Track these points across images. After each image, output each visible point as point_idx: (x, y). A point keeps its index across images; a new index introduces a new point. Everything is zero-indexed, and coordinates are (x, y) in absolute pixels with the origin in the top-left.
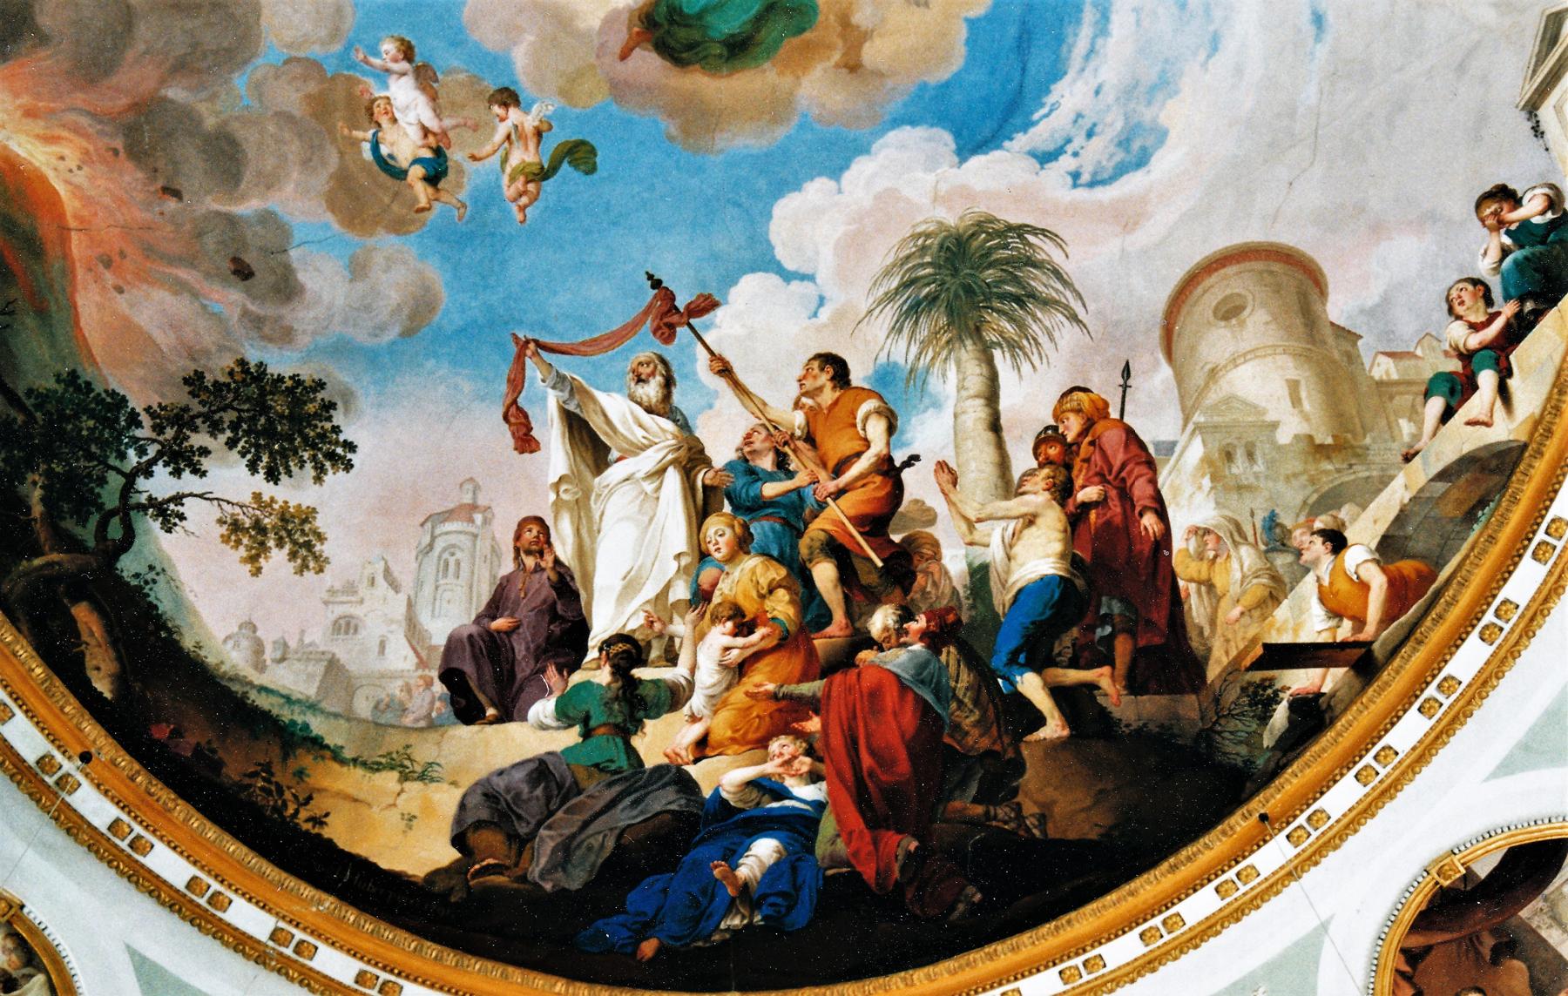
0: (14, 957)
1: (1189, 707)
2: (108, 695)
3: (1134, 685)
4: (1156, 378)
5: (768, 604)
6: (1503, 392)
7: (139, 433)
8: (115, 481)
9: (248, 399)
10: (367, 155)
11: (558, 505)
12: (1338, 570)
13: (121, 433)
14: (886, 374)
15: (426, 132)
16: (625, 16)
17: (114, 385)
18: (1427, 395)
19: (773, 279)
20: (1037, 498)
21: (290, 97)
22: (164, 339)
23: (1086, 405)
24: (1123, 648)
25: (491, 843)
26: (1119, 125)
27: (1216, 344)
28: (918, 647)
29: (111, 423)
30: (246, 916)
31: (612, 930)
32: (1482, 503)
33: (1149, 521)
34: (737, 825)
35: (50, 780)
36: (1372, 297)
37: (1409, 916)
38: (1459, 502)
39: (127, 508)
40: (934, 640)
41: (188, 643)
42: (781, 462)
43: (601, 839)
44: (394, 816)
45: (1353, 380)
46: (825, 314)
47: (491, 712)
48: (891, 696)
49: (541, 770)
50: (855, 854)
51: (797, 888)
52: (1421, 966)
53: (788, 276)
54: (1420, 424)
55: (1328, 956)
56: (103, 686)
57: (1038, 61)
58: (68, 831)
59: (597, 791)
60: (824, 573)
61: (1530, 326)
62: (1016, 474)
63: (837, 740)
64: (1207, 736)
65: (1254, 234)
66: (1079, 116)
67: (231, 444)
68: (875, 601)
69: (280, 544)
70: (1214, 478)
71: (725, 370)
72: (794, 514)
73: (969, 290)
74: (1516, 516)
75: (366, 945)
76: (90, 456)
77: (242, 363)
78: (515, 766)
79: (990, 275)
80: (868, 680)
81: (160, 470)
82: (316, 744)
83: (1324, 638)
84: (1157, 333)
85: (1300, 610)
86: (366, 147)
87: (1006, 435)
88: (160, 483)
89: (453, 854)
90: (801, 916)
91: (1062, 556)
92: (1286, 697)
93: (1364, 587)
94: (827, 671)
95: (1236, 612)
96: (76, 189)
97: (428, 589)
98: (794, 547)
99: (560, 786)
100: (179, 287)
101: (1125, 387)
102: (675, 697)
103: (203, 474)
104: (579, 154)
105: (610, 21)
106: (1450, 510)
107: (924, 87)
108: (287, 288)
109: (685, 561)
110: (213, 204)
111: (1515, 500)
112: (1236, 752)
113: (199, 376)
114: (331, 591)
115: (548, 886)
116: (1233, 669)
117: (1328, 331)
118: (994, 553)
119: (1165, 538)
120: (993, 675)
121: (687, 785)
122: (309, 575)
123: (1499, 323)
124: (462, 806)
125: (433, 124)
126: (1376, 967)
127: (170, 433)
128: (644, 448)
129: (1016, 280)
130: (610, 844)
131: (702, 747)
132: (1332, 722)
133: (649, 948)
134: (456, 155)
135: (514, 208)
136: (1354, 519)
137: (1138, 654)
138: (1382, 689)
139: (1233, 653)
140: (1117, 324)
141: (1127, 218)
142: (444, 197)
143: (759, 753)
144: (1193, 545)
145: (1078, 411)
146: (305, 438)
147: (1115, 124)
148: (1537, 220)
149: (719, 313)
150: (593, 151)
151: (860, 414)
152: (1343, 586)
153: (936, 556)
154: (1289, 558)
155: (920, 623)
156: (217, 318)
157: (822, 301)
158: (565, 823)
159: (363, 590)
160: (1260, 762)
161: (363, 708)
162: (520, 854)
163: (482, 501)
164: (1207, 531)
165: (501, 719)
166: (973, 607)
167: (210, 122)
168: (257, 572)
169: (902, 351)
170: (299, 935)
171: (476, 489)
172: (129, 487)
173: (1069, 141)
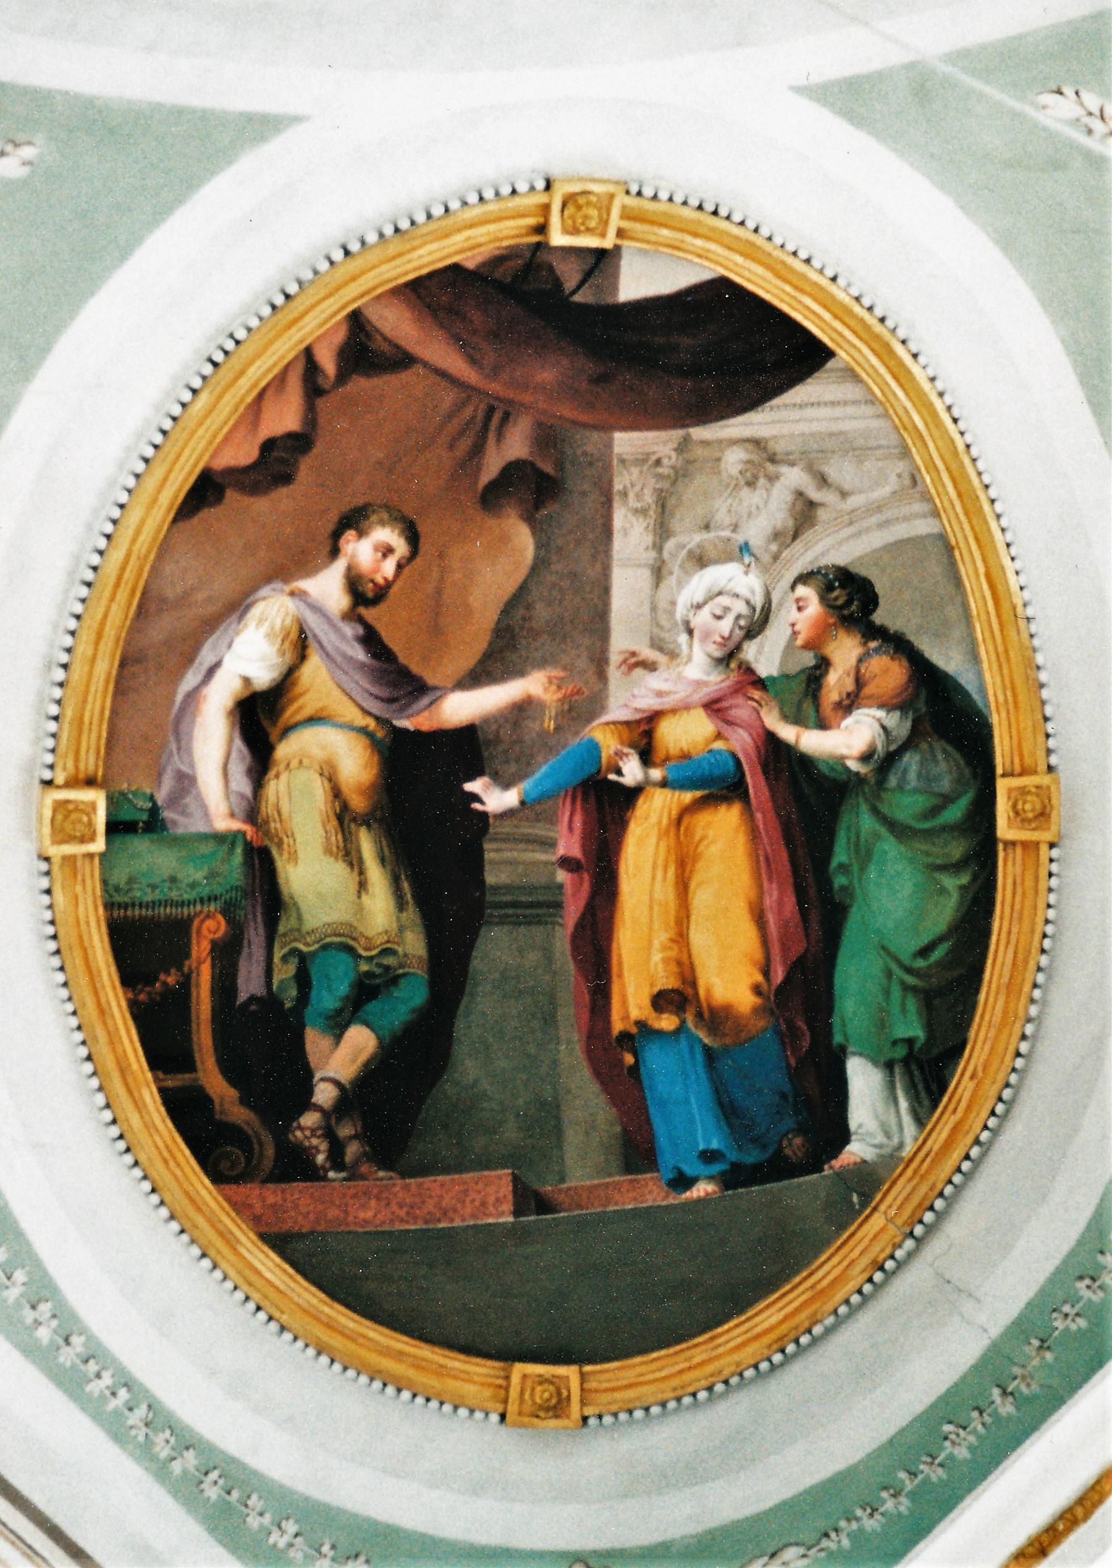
52: (360, 384)
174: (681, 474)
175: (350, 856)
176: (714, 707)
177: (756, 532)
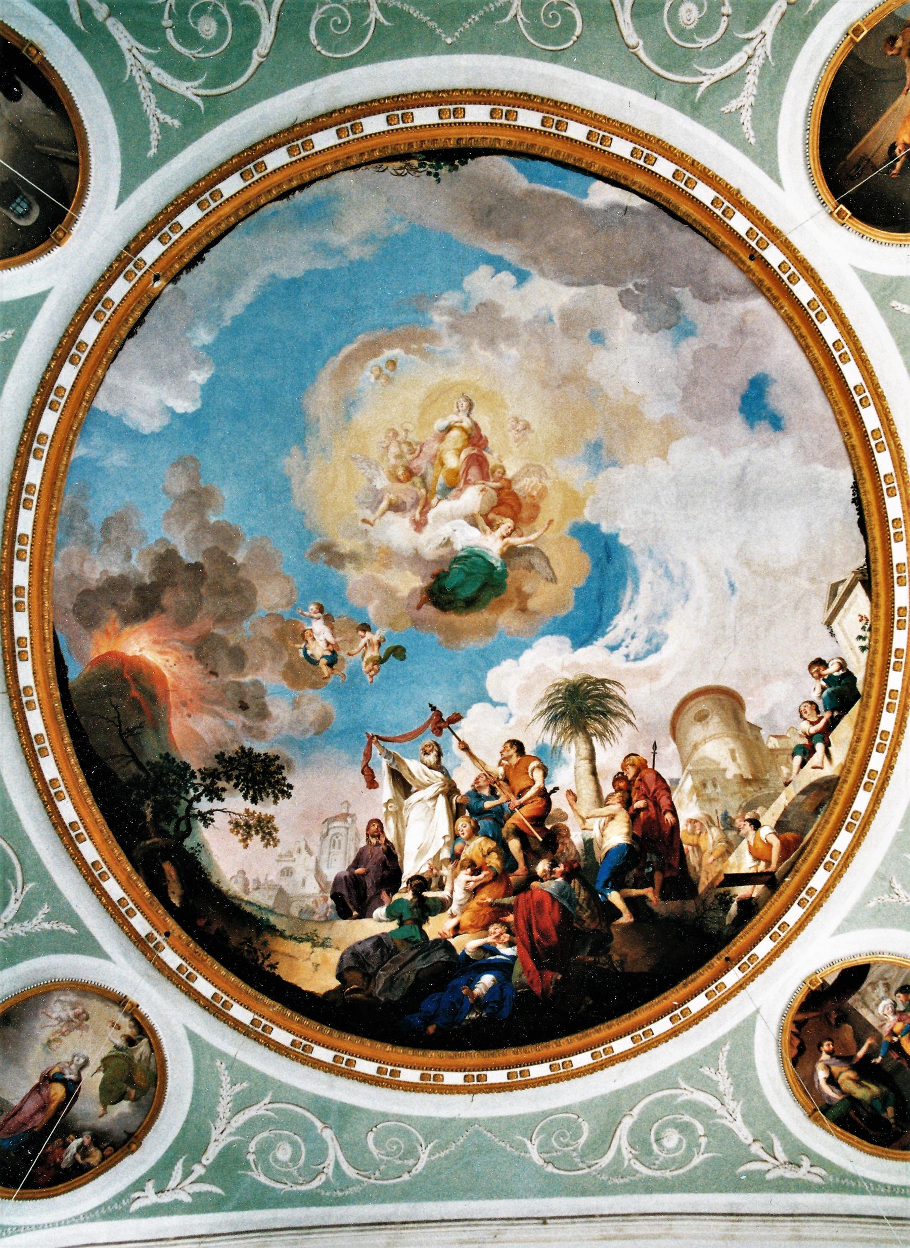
1: (690, 906)
2: (178, 905)
3: (664, 896)
4: (669, 749)
5: (487, 860)
6: (827, 753)
7: (195, 781)
8: (184, 804)
9: (244, 765)
10: (302, 655)
11: (387, 813)
12: (757, 838)
13: (188, 781)
14: (542, 749)
15: (328, 644)
16: (418, 592)
17: (185, 759)
18: (793, 755)
19: (488, 706)
20: (615, 807)
21: (268, 631)
22: (208, 738)
23: (637, 763)
24: (658, 878)
25: (355, 977)
26: (646, 633)
27: (696, 733)
28: (560, 879)
29: (182, 777)
30: (240, 1013)
31: (416, 1020)
32: (821, 805)
33: (668, 817)
34: (473, 968)
35: (152, 945)
36: (765, 711)
37: (796, 1005)
38: (811, 804)
39: (189, 816)
40: (568, 876)
41: (214, 880)
42: (493, 791)
43: (409, 975)
44: (309, 964)
45: (759, 749)
46: (513, 721)
47: (355, 913)
48: (547, 904)
49: (379, 941)
50: (532, 982)
51: (503, 999)
52: (803, 1030)
53: (495, 704)
54: (791, 768)
55: (760, 1026)
56: (176, 901)
57: (608, 606)
58: (159, 970)
59: (406, 953)
60: (514, 845)
61: (837, 722)
62: (605, 795)
63: (521, 924)
64: (700, 918)
65: (710, 682)
66: (627, 630)
67: (236, 786)
68: (539, 858)
69: (257, 833)
70: (698, 796)
71: (466, 748)
72: (499, 816)
73: (580, 709)
74: (837, 810)
75: (295, 1027)
76: (173, 792)
77: (242, 748)
78: (367, 940)
79: (590, 702)
80: (536, 895)
81: (204, 798)
82: (272, 929)
83: (752, 871)
84: (668, 731)
85: (740, 858)
86: (301, 651)
87: (600, 777)
88: (204, 805)
89: (338, 983)
90: (506, 1012)
91: (628, 834)
92: (736, 900)
93: (770, 845)
94: (516, 893)
95: (711, 859)
96: (173, 674)
97: (325, 856)
98: (500, 832)
99: (389, 949)
100: (216, 714)
101: (654, 754)
102: (443, 906)
103: (223, 800)
104: (398, 652)
105: (413, 592)
106: (807, 808)
107: (556, 618)
108: (263, 714)
109: (448, 839)
110: (231, 678)
111: (836, 803)
112: (714, 927)
113: (223, 754)
114: (281, 856)
115: (382, 999)
116: (711, 886)
117: (746, 726)
118: (595, 834)
119: (676, 827)
120: (596, 893)
121: (450, 948)
122: (270, 848)
123: (823, 722)
124: (341, 959)
125: (330, 639)
126: (782, 1030)
127: (208, 781)
128: (428, 786)
129: (601, 704)
130: (412, 977)
131: (457, 930)
132: (759, 910)
133: (431, 1029)
134: (342, 654)
135: (368, 677)
136: (763, 813)
137: (665, 882)
138: (780, 895)
139: (710, 879)
140: (649, 724)
141: (653, 675)
142: (336, 672)
143: (484, 932)
144: (689, 828)
145: (633, 765)
146: (270, 782)
147: (643, 633)
148: (836, 674)
149: (463, 722)
150: (404, 650)
151: (530, 768)
152: (760, 846)
153: (568, 835)
154: (735, 833)
155: (561, 868)
156: (231, 728)
157: (511, 715)
158: (392, 968)
159: (295, 856)
160: (725, 932)
161: (295, 912)
162: (369, 983)
163: (351, 811)
164: (696, 821)
165: (360, 917)
166: (586, 860)
167: (232, 643)
168: (246, 846)
169: (549, 738)
170: (264, 1022)
171: (349, 805)
172: (190, 807)
173: (623, 641)
174: (863, 998)
175: (863, 1086)
176: (899, 1021)
177: (882, 994)
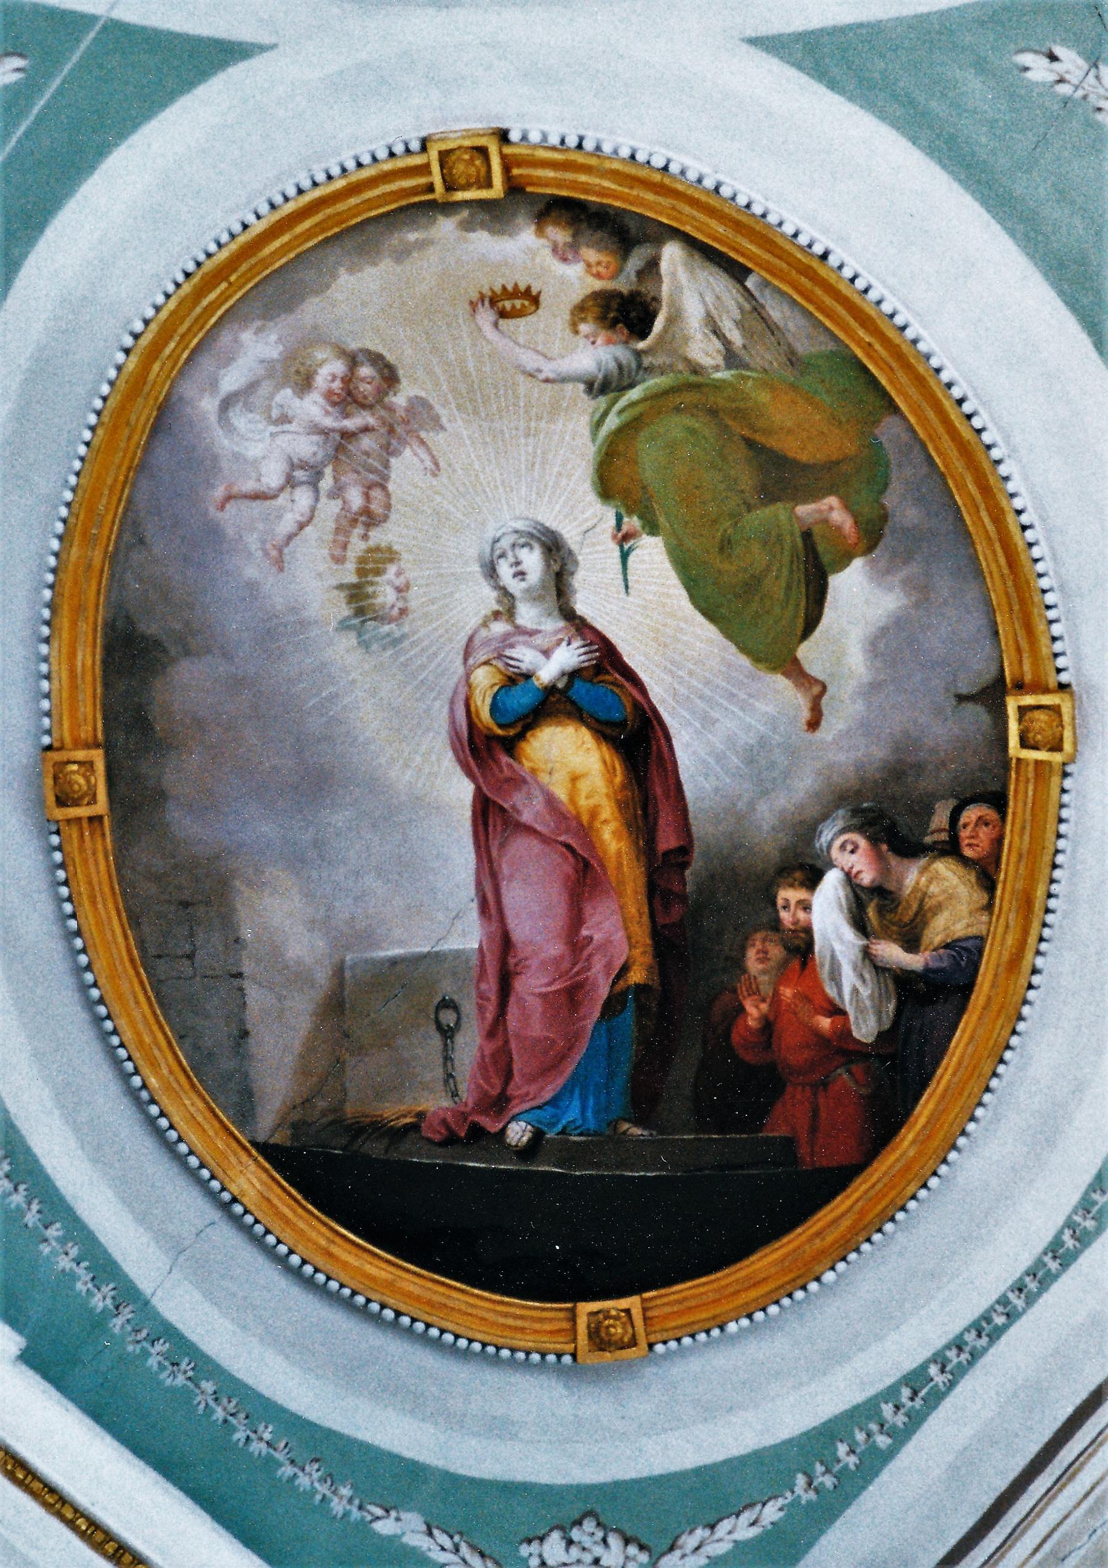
0: (591, 254)
